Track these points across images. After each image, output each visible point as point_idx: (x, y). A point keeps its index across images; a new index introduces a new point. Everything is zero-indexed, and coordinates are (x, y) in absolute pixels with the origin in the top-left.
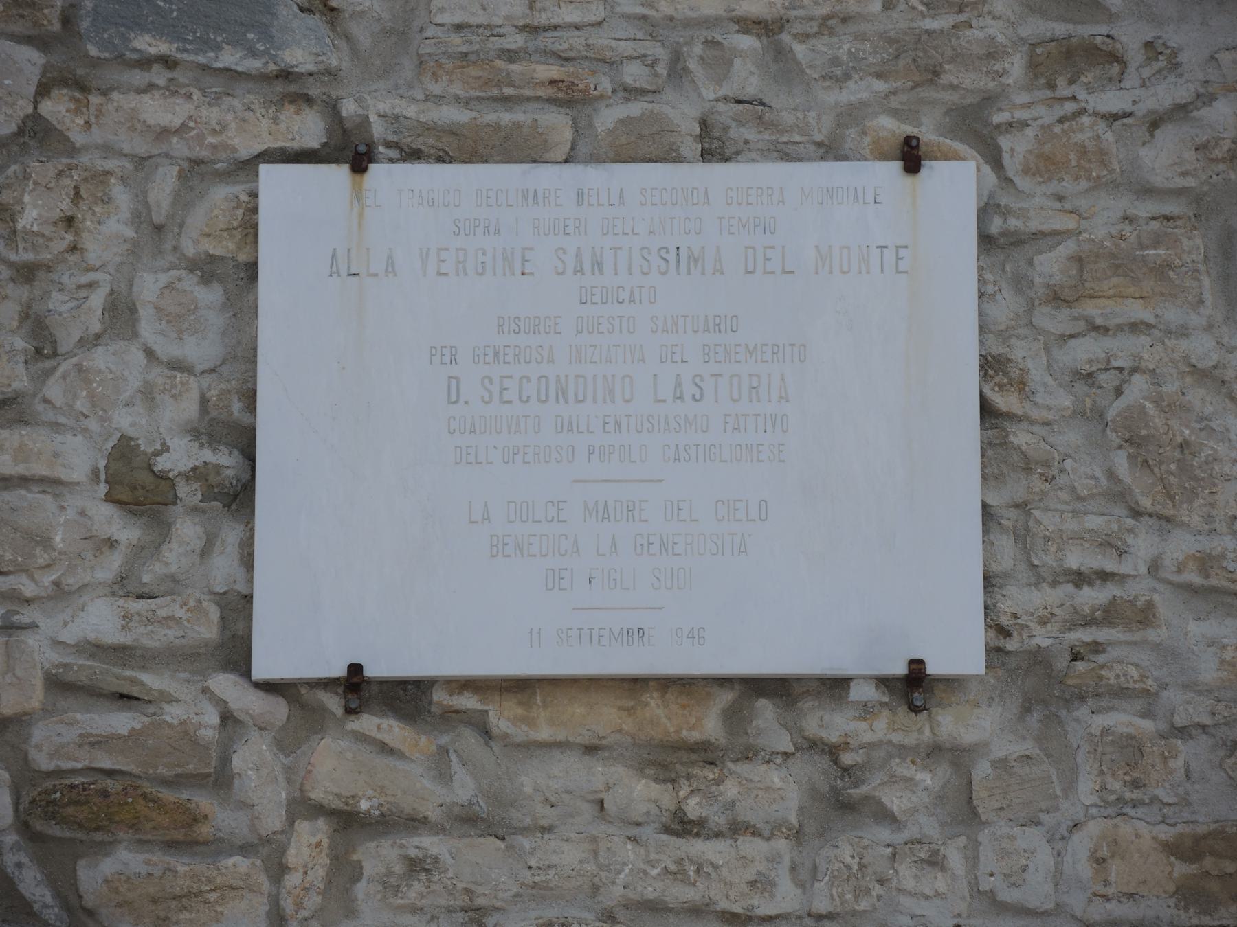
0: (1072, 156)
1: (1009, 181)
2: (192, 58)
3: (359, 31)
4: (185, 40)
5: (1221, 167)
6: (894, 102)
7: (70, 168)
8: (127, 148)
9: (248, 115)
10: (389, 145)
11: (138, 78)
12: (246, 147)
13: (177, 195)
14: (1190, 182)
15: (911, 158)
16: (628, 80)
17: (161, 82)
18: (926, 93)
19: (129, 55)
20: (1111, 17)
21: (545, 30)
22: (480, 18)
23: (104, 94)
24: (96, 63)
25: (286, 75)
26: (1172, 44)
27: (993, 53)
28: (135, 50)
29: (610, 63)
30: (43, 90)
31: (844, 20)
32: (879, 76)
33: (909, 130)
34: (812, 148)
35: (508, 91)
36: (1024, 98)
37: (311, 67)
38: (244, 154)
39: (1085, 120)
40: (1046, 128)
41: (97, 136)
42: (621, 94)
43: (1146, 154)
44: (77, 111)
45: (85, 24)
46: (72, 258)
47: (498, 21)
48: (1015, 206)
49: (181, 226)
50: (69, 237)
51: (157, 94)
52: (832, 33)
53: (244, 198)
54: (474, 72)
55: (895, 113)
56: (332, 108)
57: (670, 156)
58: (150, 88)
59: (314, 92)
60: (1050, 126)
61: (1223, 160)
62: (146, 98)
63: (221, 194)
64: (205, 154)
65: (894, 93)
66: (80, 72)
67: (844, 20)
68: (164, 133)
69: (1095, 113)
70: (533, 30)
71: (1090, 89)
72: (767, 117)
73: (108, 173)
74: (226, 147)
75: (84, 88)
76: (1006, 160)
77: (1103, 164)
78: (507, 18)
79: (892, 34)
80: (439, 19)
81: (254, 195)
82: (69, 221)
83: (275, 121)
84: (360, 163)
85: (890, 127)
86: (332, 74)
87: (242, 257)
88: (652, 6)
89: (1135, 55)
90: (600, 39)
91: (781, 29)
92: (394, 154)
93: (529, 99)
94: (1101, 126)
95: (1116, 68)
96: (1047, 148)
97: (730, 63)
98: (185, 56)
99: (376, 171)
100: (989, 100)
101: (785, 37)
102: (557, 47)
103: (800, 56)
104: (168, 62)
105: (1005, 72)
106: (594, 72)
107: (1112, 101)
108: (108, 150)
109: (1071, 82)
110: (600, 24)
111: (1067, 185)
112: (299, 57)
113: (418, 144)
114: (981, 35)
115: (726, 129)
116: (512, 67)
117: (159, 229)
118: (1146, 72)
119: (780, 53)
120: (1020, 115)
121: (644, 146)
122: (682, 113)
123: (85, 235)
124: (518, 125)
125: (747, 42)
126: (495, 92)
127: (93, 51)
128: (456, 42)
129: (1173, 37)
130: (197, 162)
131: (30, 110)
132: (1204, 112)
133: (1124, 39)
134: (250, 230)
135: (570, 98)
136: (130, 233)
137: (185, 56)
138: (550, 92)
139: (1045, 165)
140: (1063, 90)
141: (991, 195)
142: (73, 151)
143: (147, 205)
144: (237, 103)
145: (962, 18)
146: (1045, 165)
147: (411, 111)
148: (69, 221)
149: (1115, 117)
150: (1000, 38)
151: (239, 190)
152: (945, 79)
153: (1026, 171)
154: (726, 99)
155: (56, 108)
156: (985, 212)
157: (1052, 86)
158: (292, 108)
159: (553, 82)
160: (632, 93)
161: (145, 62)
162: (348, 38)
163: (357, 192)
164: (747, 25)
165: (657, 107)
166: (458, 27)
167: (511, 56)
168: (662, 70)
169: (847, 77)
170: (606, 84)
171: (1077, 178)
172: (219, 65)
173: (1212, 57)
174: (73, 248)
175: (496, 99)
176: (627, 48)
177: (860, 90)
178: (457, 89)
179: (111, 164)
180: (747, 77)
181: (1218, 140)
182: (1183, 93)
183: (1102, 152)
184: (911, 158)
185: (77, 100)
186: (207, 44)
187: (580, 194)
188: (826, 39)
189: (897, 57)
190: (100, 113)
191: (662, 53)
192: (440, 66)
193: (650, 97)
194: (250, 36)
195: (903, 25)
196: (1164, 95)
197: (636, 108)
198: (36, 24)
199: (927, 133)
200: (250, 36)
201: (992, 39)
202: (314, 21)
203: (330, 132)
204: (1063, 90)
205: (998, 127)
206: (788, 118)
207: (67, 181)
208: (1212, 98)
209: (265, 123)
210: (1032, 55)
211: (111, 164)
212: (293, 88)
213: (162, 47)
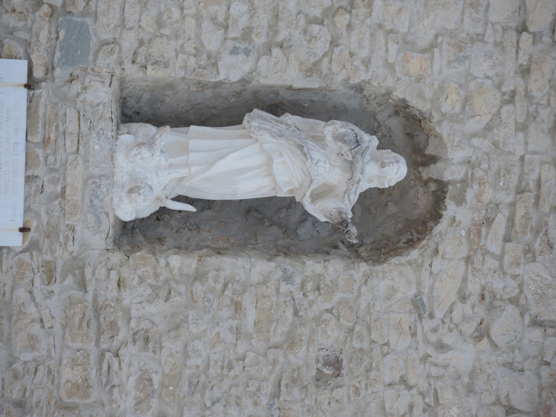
0: (22, 271)
1: (17, 255)
2: (58, 44)
3: (66, 87)
4: (63, 43)
5: (18, 309)
6: (41, 226)
7: (28, 12)
8: (34, 26)
9: (42, 58)
10: (33, 94)
11: (53, 30)
12: (33, 57)
13: (21, 38)
14: (14, 301)
15: (24, 230)
16: (49, 157)
17: (52, 36)
18: (43, 234)
19: (59, 28)
20: (61, 282)
21: (64, 137)
22: (68, 120)
23: (49, 21)
24: (57, 19)
25: (53, 68)
26: (52, 298)
27: (52, 252)
28: (60, 30)
29: (55, 153)
30: (50, 6)
31: (64, 214)
32: (48, 222)
33: (32, 230)
34: (29, 204)
35: (47, 126)
36: (40, 259)
37: (55, 75)
38: (31, 56)
39: (32, 275)
40: (31, 265)
41: (38, 19)
42: (46, 156)
43: (22, 290)
44: (44, 14)
45: (68, 17)
46: (4, 11)
47: (67, 124)
48: (10, 256)
49: (13, 39)
50: (10, 10)
51: (48, 35)
52: (61, 211)
53: (19, 56)
54: (53, 117)
55: (38, 227)
56: (44, 80)
57: (27, 165)
58: (50, 33)
59: (49, 75)
60: (31, 266)
61: (20, 309)
62: (47, 32)
63: (21, 50)
64: (32, 46)
65: (43, 226)
66: (55, 15)
67: (64, 214)
68: (38, 36)
69: (34, 277)
70: (64, 133)
71: (41, 276)
72: (38, 193)
73: (27, 21)
74: (33, 52)
75: (51, 16)
76: (22, 254)
77: (20, 279)
78: (68, 127)
79: (59, 226)
80: (68, 109)
81: (20, 58)
82: (14, 11)
83: (41, 65)
84: (28, 86)
85: (33, 225)
86: (54, 80)
87: (3, 55)
88: (70, 164)
89: (50, 288)
90: (61, 151)
91: (63, 198)
92: (31, 95)
93: (45, 131)
94: (30, 279)
95: (46, 283)
96: (25, 265)
97: (53, 184)
98: (58, 43)
99: (25, 90)
100: (40, 250)
101: (60, 199)
102: (59, 139)
103: (54, 202)
104: (57, 38)
105: (47, 255)
106: (52, 148)
107: (37, 282)
108: (34, 21)
109: (43, 272)
110: (65, 151)
111: (14, 270)
112: (58, 72)
113: (33, 102)
114: (58, 249)
115: (35, 182)
116: (54, 128)
117: (12, 33)
118: (45, 291)
119: (56, 197)
120: (35, 258)
121: (30, 160)
122: (40, 171)
123: (10, 14)
124: (38, 128)
125: (59, 189)
126: (47, 123)
127: (60, 19)
128: (61, 113)
129: (54, 298)
130: (30, 44)
131: (45, 2)
132: (33, 305)
133: (55, 285)
134: (10, 57)
135: (45, 142)
136: (11, 26)
137: (58, 43)
138: (47, 137)
139: (21, 264)
140: (41, 270)
141: (13, 250)
142: (34, 12)
143: (19, 31)
144: (45, 55)
145: (63, 244)
146: (21, 264)
147: (42, 100)
148: (14, 11)
149: (33, 282)
150: (56, 254)
151: (22, 54)
152: (46, 239)
153: (19, 259)
154: (43, 183)
155: (45, 9)
156: (9, 249)
157: (43, 266)
158: (44, 69)
159: (49, 138)
160: (46, 158)
161: (57, 32)
162: (64, 85)
163: (20, 85)
164: (64, 189)
165: (42, 164)
166: (65, 114)
167: (57, 127)
168: (52, 166)
169: (48, 214)
170: (49, 152)
171: (16, 272)
172: (56, 51)
173: (47, 307)
174: (7, 11)
175: (45, 122)
176: (59, 158)
177: (44, 218)
178: (48, 113)
179: (29, 22)
180: (49, 188)
181: (25, 308)
182: (38, 300)
183: (23, 279)
184: (24, 230)
185: (48, 14)
186: (62, 49)
187: (17, 143)
188: (59, 209)
189: (53, 227)
190: (44, 20)
191: (58, 165)
192: (55, 108)
193: (45, 163)
194: (64, 60)
195: (62, 229)
196: (38, 295)
197: (42, 159)
198: (69, 4)
199: (31, 234)
200: (64, 60)
201: (56, 252)
202: (68, 77)
203: (38, 79)
204: (41, 270)
205: (32, 252)
206: (37, 199)
207: (24, 11)
208: (37, 307)
209: (40, 62)
210: (51, 262)
211: (29, 22)
212: (50, 70)
213: (61, 36)
